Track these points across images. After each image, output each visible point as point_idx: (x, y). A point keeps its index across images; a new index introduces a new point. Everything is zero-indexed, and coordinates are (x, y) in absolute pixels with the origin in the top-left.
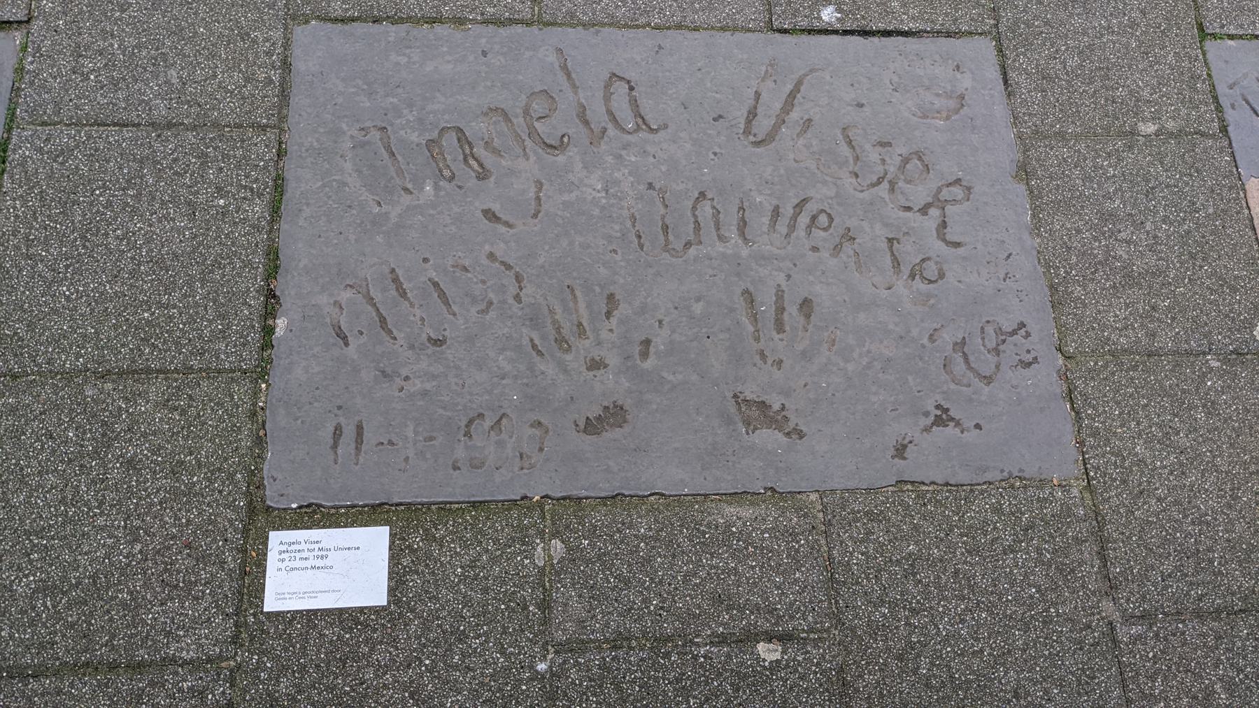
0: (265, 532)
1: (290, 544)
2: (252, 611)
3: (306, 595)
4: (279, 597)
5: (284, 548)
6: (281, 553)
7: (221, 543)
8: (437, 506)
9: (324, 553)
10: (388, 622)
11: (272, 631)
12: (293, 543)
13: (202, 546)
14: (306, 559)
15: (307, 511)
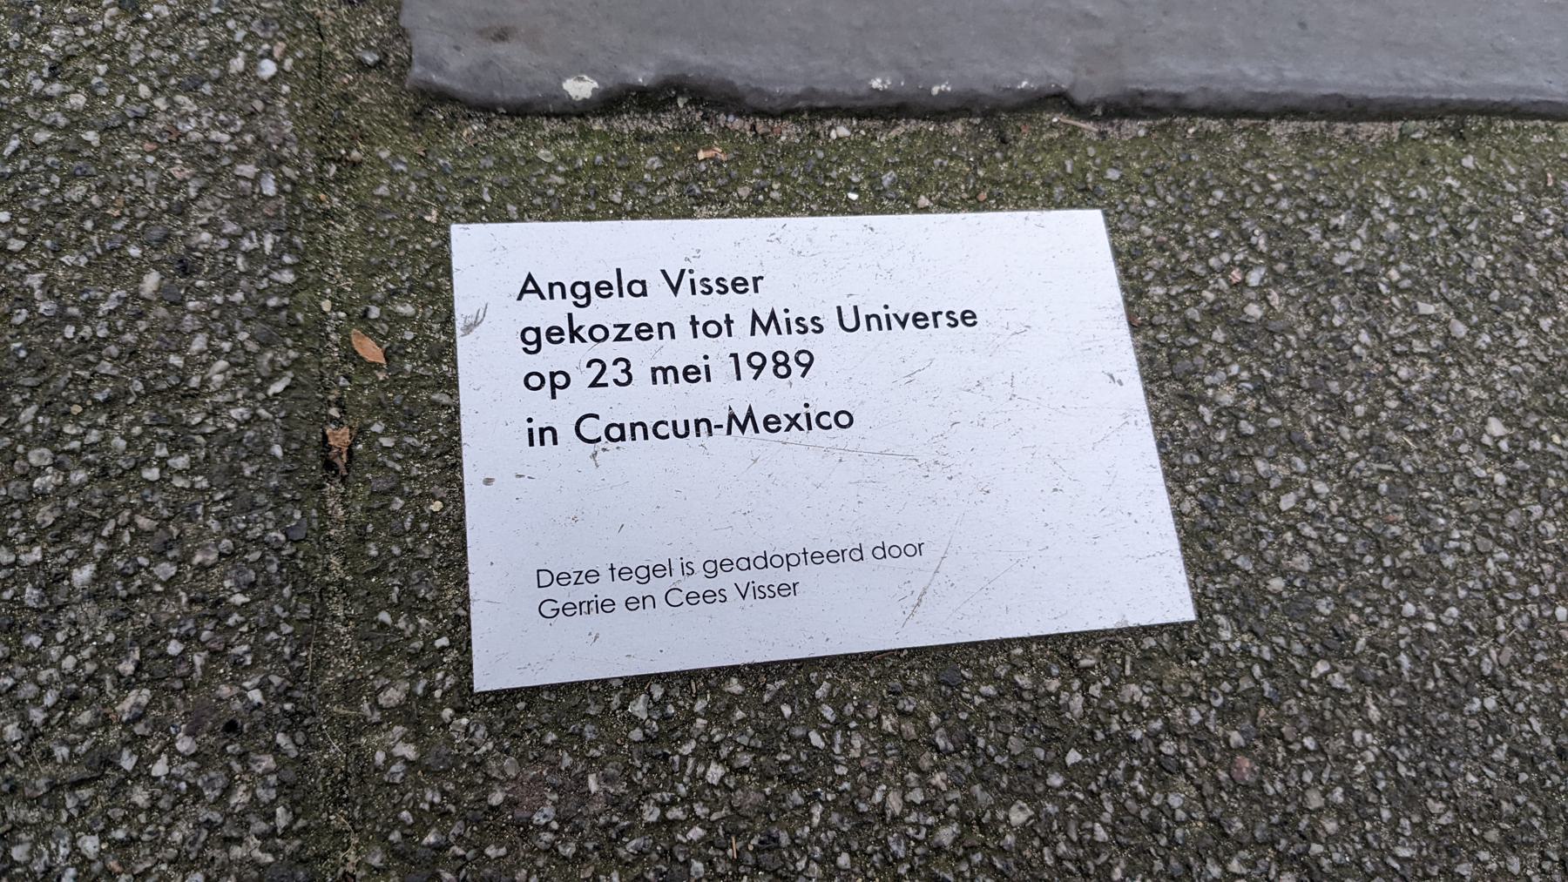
0: (422, 227)
1: (586, 293)
2: (393, 696)
3: (724, 581)
4: (562, 594)
5: (553, 312)
6: (533, 340)
7: (151, 281)
8: (1291, 127)
9: (791, 343)
10: (1228, 714)
11: (544, 815)
12: (603, 289)
13: (27, 300)
14: (691, 373)
15: (649, 127)
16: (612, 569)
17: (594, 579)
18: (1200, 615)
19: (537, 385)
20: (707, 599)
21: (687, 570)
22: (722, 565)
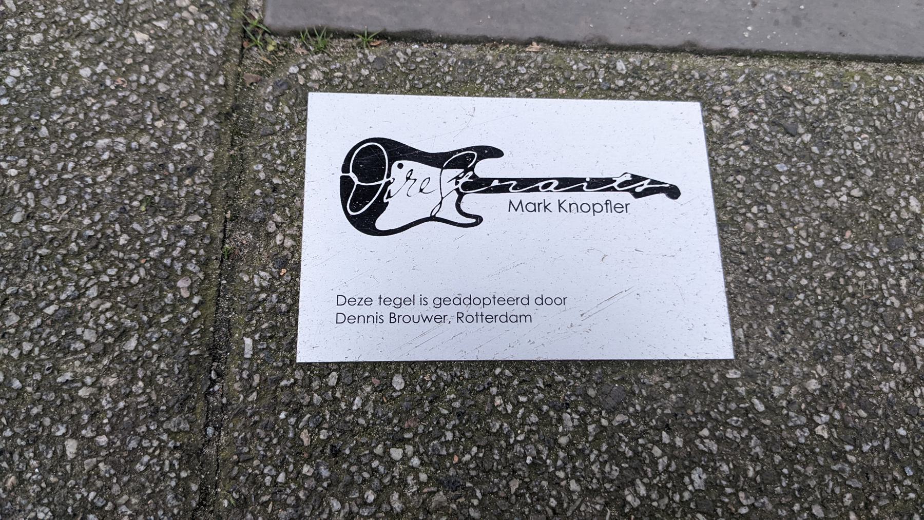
4: (348, 310)
16: (380, 298)
17: (369, 303)
18: (736, 356)
19: (463, 207)
20: (406, 303)
21: (423, 302)
22: (443, 301)
